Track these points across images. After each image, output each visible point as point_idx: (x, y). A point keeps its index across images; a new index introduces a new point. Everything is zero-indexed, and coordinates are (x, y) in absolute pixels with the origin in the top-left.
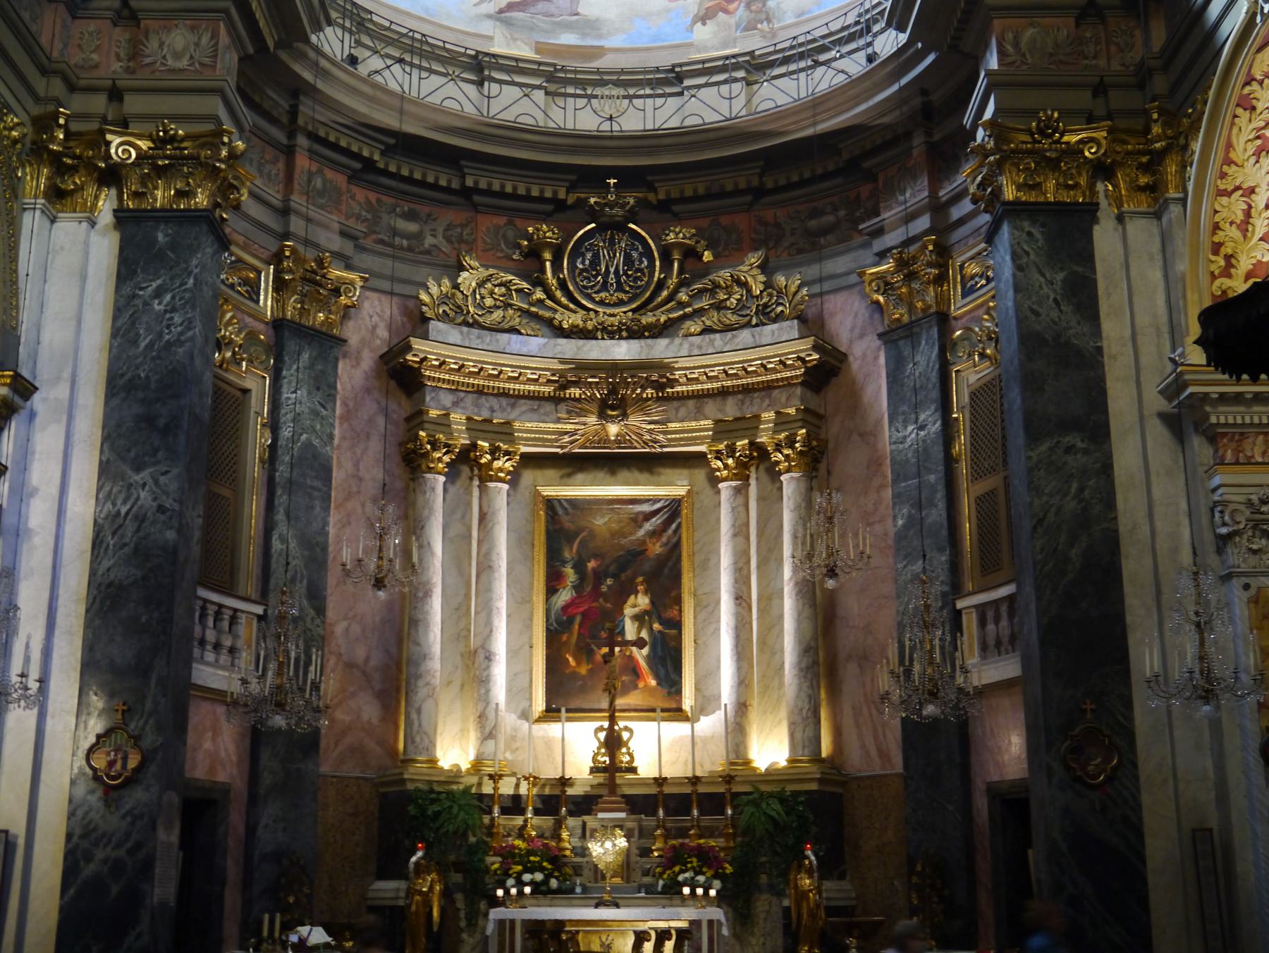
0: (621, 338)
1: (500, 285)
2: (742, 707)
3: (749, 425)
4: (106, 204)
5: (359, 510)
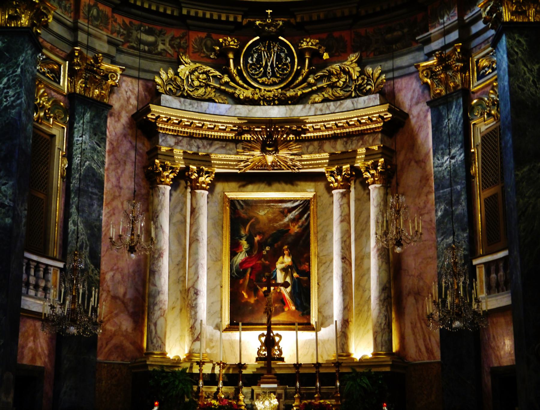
0: (275, 104)
1: (203, 73)
2: (346, 323)
3: (351, 156)
5: (120, 206)
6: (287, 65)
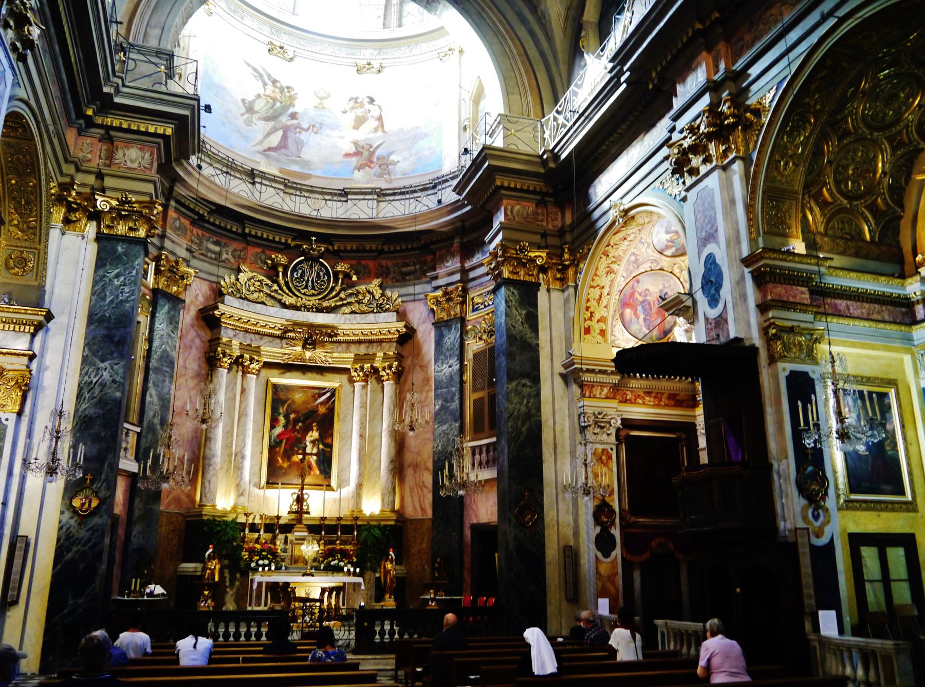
0: (313, 311)
1: (258, 281)
2: (359, 486)
3: (370, 357)
4: (91, 229)
5: (185, 383)
6: (324, 281)
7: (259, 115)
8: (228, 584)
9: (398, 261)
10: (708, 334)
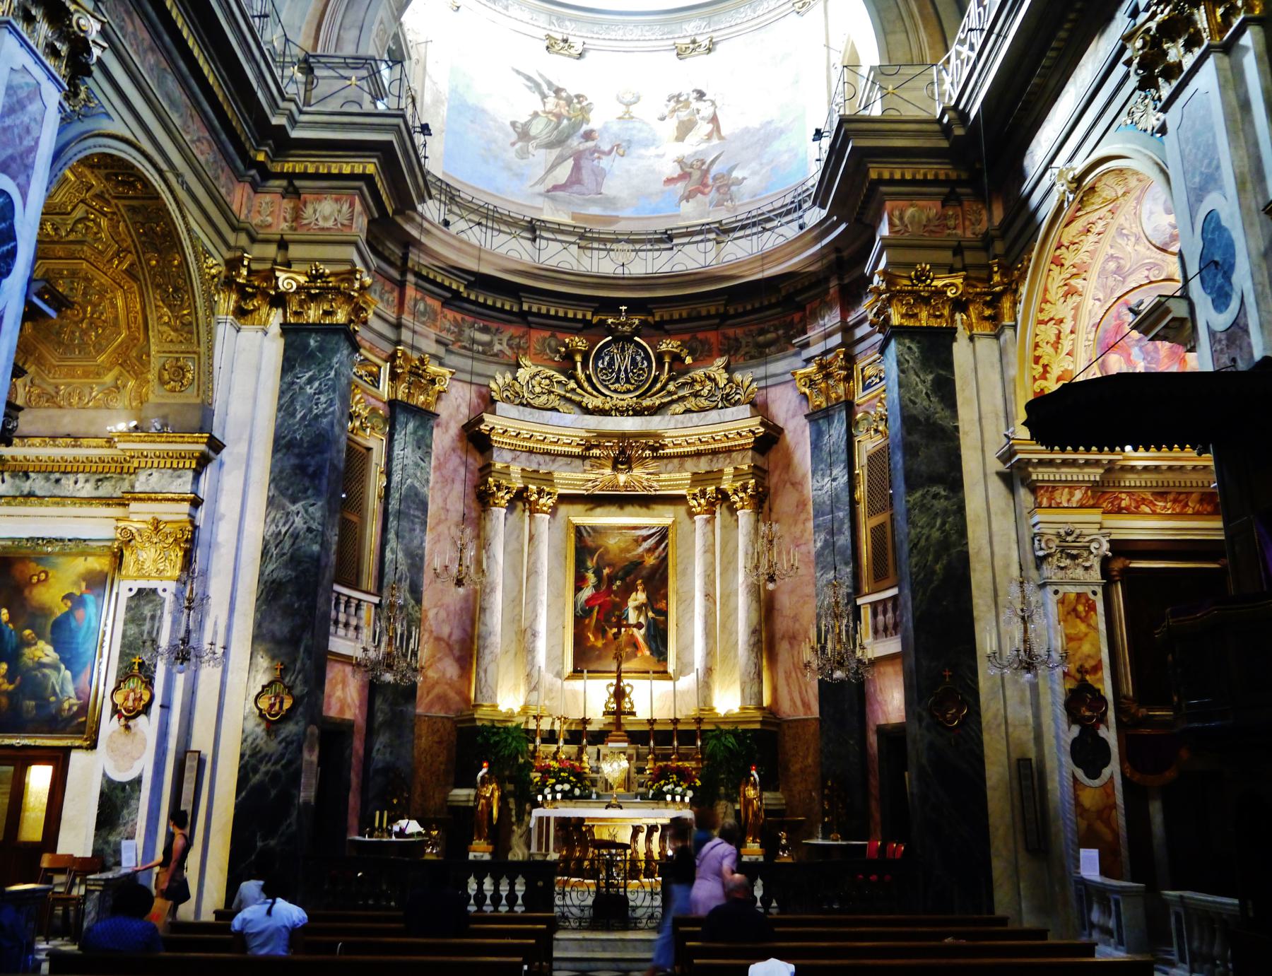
0: (628, 415)
1: (546, 378)
2: (709, 671)
3: (716, 476)
4: (276, 318)
5: (446, 532)
6: (643, 369)
7: (538, 141)
8: (514, 819)
9: (752, 328)
10: (1215, 360)
